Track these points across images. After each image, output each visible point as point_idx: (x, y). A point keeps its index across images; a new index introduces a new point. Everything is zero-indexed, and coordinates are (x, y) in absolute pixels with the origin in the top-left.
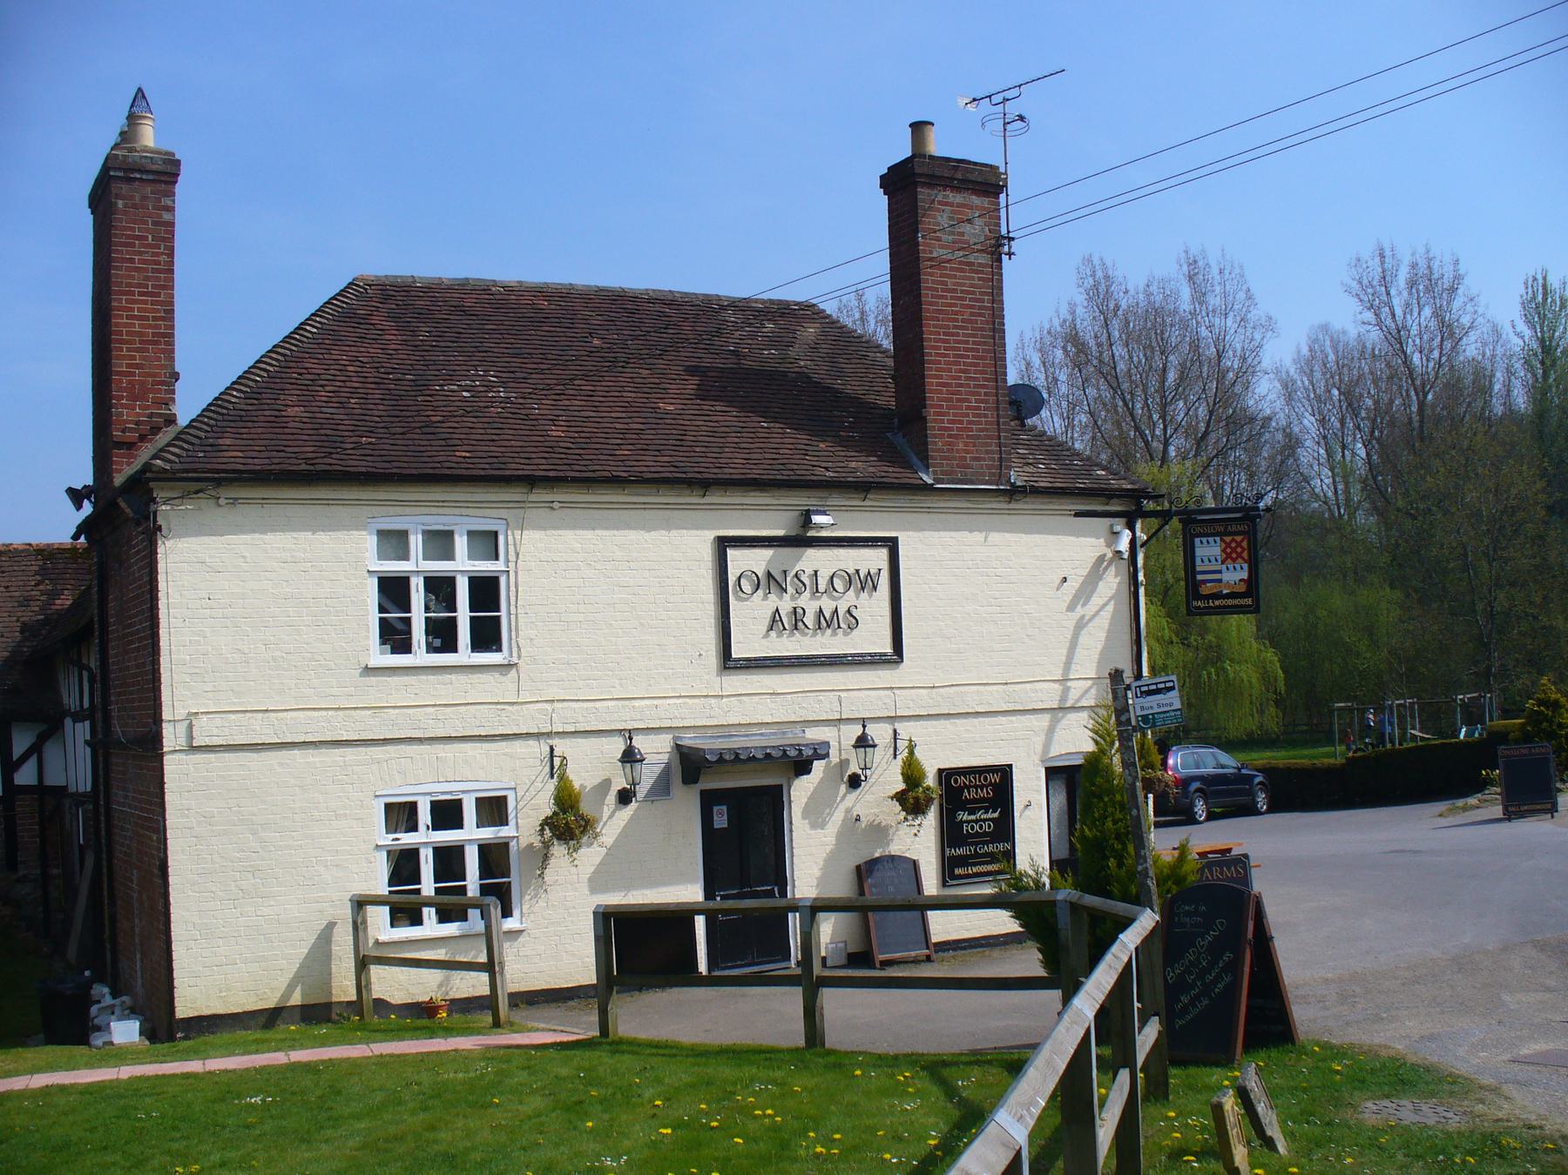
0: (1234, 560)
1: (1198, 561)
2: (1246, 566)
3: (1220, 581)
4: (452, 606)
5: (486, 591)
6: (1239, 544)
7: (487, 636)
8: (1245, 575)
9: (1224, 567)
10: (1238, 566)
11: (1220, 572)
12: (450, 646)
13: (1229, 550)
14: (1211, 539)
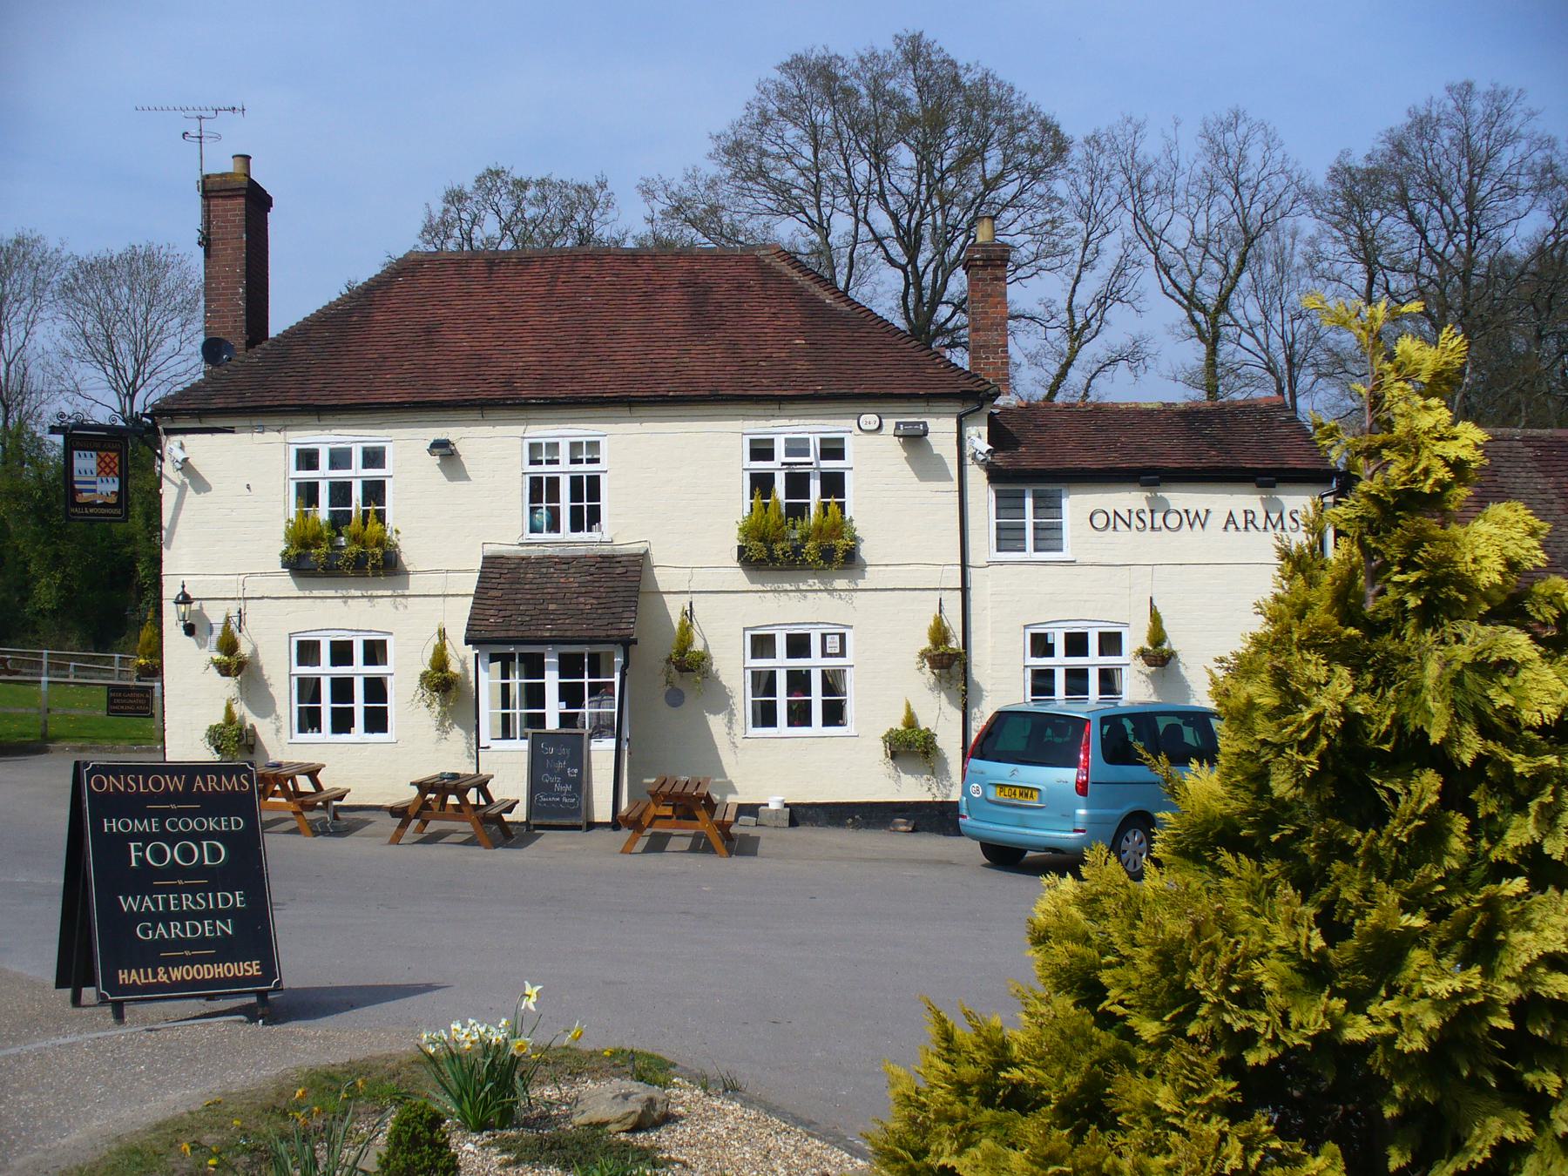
0: (108, 474)
1: (76, 472)
2: (117, 480)
3: (95, 491)
4: (807, 691)
5: (832, 683)
6: (112, 460)
7: (834, 714)
8: (115, 488)
9: (99, 480)
10: (110, 479)
11: (95, 483)
12: (806, 721)
13: (103, 465)
14: (88, 453)
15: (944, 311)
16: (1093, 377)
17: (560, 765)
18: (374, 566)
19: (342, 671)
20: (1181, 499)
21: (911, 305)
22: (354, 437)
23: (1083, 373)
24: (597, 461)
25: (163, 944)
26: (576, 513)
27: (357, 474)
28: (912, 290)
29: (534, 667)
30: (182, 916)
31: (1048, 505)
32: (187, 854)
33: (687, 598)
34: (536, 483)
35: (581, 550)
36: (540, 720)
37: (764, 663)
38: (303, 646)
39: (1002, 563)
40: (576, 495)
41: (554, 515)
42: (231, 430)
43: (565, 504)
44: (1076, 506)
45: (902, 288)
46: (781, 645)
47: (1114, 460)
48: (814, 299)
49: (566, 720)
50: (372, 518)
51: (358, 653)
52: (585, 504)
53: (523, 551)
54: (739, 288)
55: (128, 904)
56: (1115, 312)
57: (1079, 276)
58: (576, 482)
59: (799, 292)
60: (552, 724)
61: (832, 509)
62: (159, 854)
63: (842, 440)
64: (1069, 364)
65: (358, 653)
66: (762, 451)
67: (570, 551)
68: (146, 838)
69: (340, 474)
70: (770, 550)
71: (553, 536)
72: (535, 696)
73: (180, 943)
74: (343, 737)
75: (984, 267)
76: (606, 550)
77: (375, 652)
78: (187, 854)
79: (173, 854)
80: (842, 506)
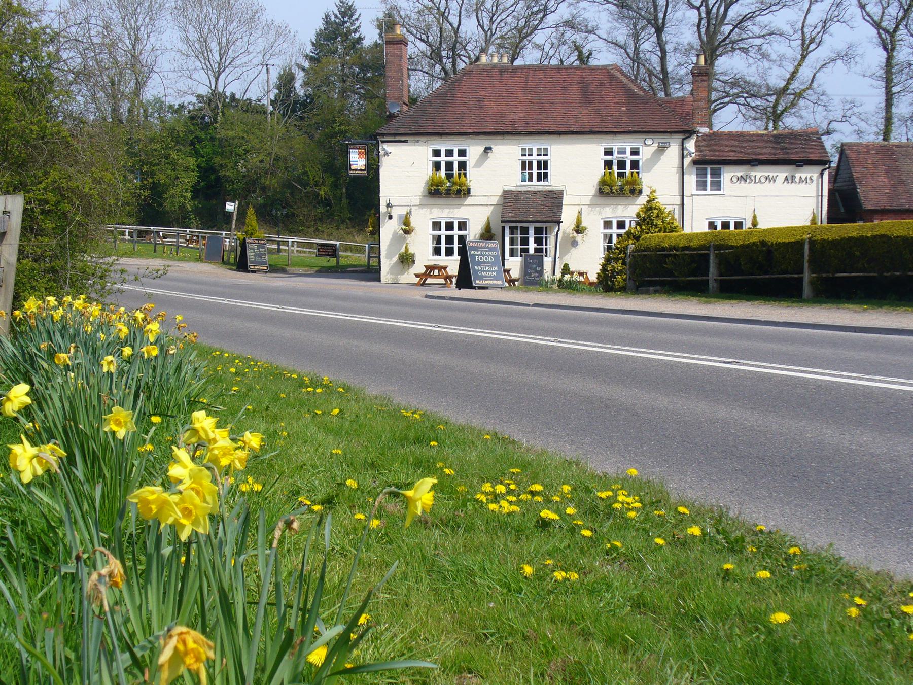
15: (727, 29)
16: (817, 72)
17: (534, 266)
18: (464, 194)
19: (450, 233)
20: (759, 173)
21: (703, 30)
22: (455, 145)
23: (811, 69)
24: (547, 155)
25: (483, 276)
26: (539, 175)
27: (456, 159)
28: (704, 22)
29: (525, 231)
30: (486, 271)
31: (716, 174)
32: (486, 259)
33: (580, 207)
34: (524, 163)
35: (540, 189)
36: (527, 250)
37: (608, 231)
38: (465, 223)
39: (698, 195)
40: (539, 168)
41: (531, 175)
42: (406, 141)
43: (535, 171)
44: (728, 175)
45: (697, 21)
46: (615, 225)
47: (742, 157)
48: (630, 90)
49: (536, 250)
50: (462, 175)
51: (456, 226)
52: (542, 171)
53: (519, 189)
54: (601, 84)
55: (477, 268)
56: (835, 28)
57: (809, 10)
58: (539, 163)
59: (624, 86)
60: (532, 251)
61: (635, 174)
62: (481, 259)
63: (639, 148)
64: (800, 65)
65: (456, 226)
66: (608, 152)
67: (537, 189)
68: (479, 255)
69: (449, 159)
70: (611, 189)
71: (530, 183)
72: (525, 241)
73: (486, 276)
74: (450, 258)
75: (698, 76)
76: (550, 189)
77: (462, 226)
78: (486, 259)
79: (484, 259)
80: (638, 173)
